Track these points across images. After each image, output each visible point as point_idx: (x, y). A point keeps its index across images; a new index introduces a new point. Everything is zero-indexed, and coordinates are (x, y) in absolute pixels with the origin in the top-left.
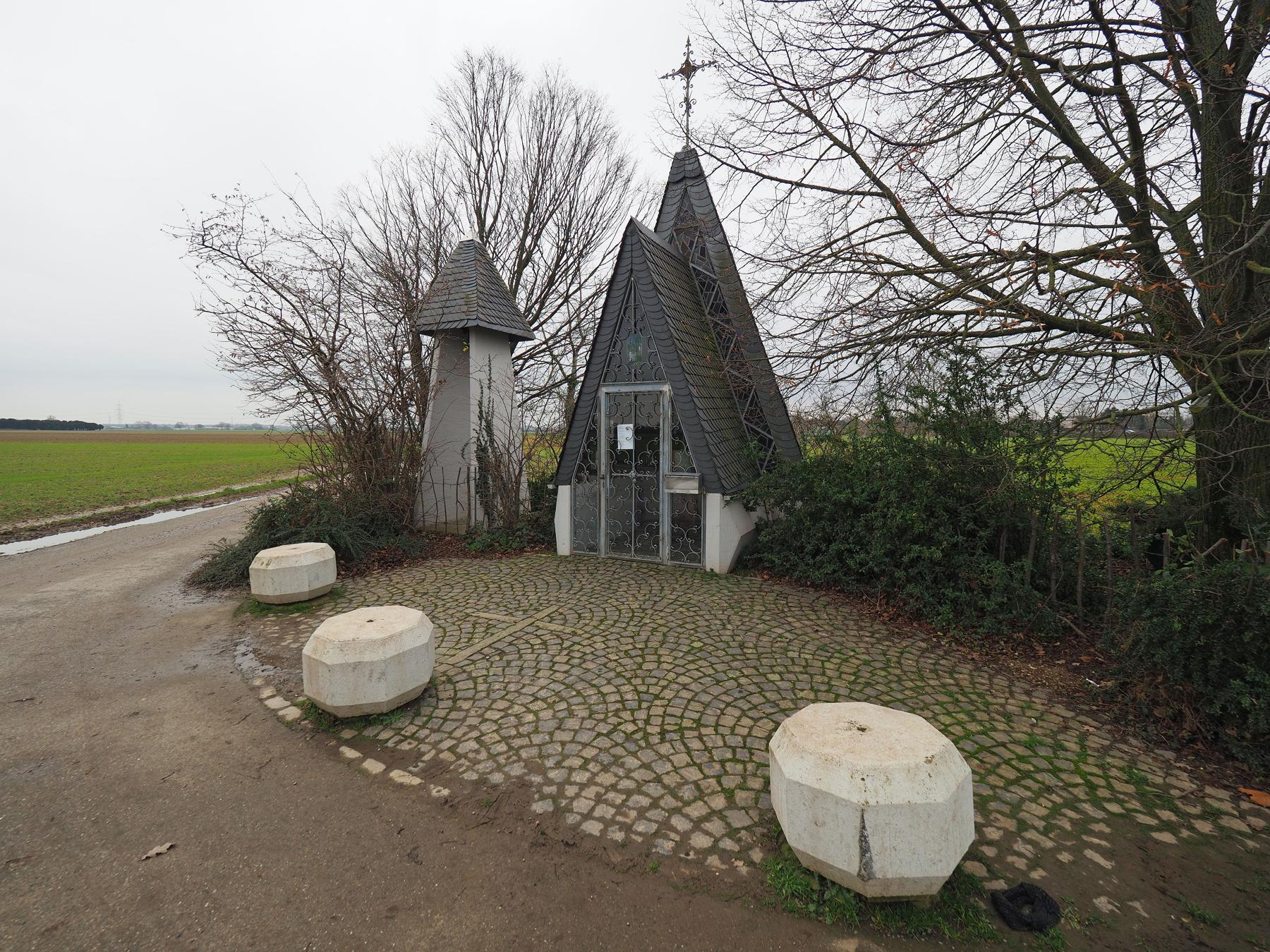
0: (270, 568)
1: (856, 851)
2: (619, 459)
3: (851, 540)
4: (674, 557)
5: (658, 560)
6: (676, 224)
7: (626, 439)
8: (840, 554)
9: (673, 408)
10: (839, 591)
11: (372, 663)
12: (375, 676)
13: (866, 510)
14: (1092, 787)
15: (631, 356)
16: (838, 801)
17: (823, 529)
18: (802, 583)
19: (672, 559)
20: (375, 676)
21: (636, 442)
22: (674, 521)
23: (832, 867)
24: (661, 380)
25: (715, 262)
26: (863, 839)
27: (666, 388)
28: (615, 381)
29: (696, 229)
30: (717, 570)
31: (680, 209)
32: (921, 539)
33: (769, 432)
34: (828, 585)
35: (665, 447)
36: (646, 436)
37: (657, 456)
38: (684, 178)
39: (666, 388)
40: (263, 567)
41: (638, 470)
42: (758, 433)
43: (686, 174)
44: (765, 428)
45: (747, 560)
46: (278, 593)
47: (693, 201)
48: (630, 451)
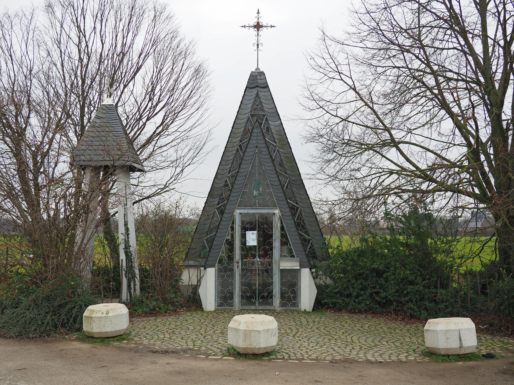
0: (109, 315)
1: (459, 341)
2: (247, 251)
3: (377, 287)
4: (282, 305)
5: (272, 308)
6: (251, 111)
7: (252, 238)
8: (371, 295)
9: (282, 223)
10: (372, 313)
11: (272, 329)
12: (273, 334)
13: (385, 272)
14: (492, 344)
15: (255, 193)
16: (453, 331)
17: (361, 283)
18: (353, 311)
19: (282, 306)
20: (273, 334)
21: (258, 241)
22: (282, 284)
23: (452, 349)
24: (274, 206)
25: (275, 136)
26: (460, 338)
27: (277, 211)
28: (246, 206)
29: (264, 116)
30: (308, 310)
31: (254, 104)
32: (411, 283)
33: (308, 235)
34: (369, 311)
35: (277, 244)
36: (265, 238)
37: (271, 249)
38: (257, 86)
39: (277, 211)
40: (104, 315)
41: (259, 257)
42: (302, 235)
43: (257, 83)
44: (306, 233)
45: (320, 305)
46: (113, 330)
47: (262, 100)
48: (255, 246)
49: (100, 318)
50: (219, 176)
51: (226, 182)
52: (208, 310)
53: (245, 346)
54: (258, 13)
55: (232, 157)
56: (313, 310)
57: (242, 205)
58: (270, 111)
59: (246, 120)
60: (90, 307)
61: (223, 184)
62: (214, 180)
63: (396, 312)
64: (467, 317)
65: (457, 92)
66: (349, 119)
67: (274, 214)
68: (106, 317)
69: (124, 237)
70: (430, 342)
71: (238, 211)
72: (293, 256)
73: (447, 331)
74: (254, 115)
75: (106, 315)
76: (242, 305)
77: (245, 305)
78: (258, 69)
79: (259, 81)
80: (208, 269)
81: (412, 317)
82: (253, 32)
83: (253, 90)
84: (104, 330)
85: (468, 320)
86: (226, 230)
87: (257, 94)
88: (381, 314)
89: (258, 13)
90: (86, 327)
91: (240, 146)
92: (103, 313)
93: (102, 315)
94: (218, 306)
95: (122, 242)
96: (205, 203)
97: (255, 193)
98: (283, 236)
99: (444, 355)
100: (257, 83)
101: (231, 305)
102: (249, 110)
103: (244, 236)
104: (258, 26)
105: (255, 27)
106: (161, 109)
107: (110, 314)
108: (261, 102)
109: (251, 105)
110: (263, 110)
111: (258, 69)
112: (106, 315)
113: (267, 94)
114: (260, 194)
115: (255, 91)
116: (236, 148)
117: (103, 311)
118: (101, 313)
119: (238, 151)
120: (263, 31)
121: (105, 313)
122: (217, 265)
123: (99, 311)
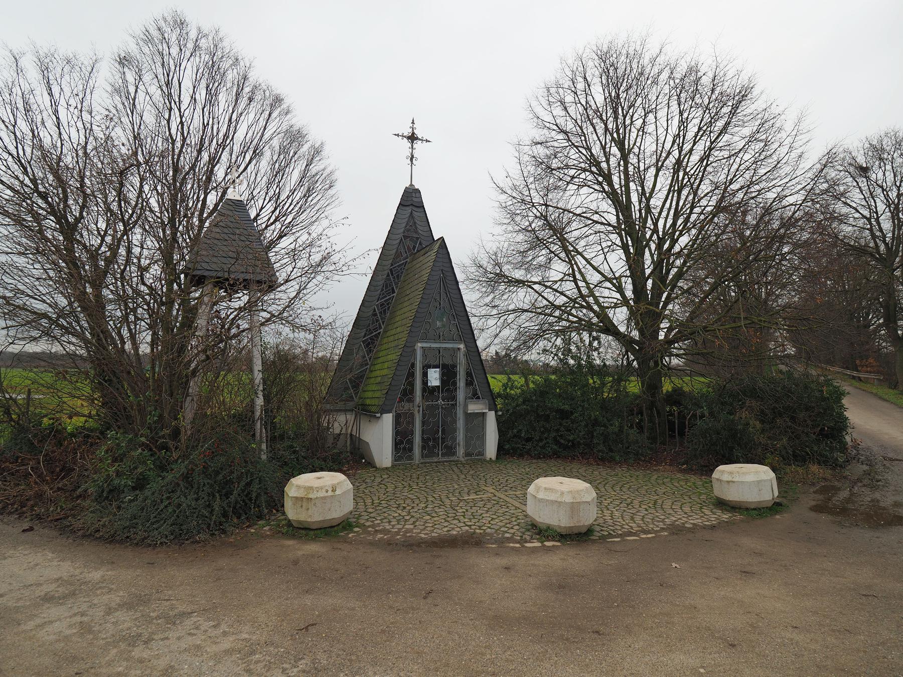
2: (429, 391)
7: (434, 378)
15: (438, 323)
16: (765, 481)
21: (442, 381)
29: (417, 239)
35: (461, 383)
36: (449, 374)
39: (462, 346)
40: (330, 493)
43: (411, 201)
45: (502, 450)
49: (324, 498)
51: (375, 310)
52: (384, 466)
53: (572, 525)
54: (413, 123)
55: (381, 283)
56: (497, 458)
57: (425, 339)
58: (425, 234)
59: (398, 241)
60: (294, 481)
61: (371, 313)
63: (583, 454)
66: (291, 278)
67: (459, 349)
68: (332, 496)
70: (719, 492)
71: (419, 345)
72: (478, 398)
73: (759, 482)
74: (408, 237)
75: (332, 494)
76: (422, 457)
77: (427, 456)
78: (411, 185)
79: (414, 199)
80: (385, 415)
81: (603, 459)
82: (406, 143)
83: (407, 208)
87: (411, 213)
88: (565, 458)
89: (413, 123)
90: (292, 512)
91: (391, 270)
92: (327, 491)
94: (396, 460)
97: (438, 323)
98: (469, 374)
99: (755, 509)
100: (411, 201)
101: (410, 458)
102: (402, 230)
103: (425, 375)
104: (412, 138)
105: (409, 138)
107: (338, 492)
108: (415, 223)
109: (404, 225)
110: (416, 232)
111: (411, 185)
112: (332, 494)
113: (398, 221)
114: (444, 326)
115: (409, 210)
116: (386, 272)
118: (324, 491)
119: (388, 275)
120: (418, 145)
121: (330, 490)
123: (322, 488)
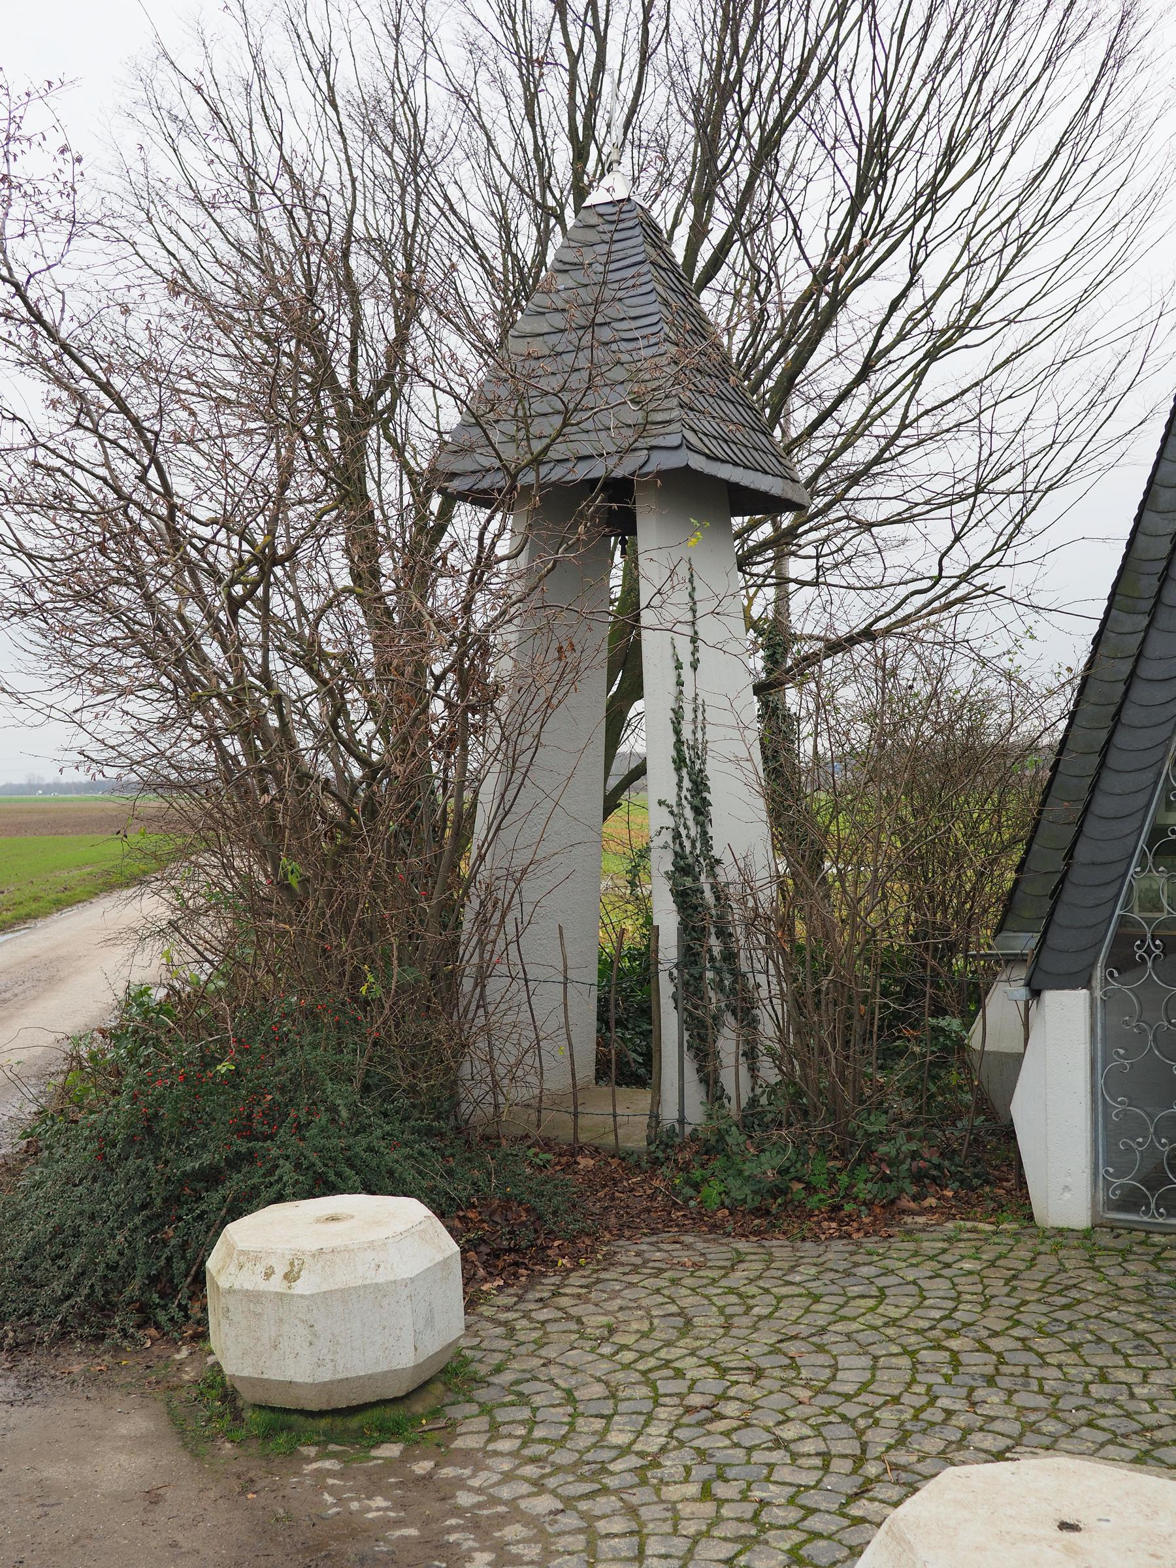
0: (301, 1287)
40: (276, 1284)
46: (325, 1375)
50: (1165, 497)
62: (1138, 520)
64: (399, 1189)
65: (541, 67)
68: (280, 1296)
69: (670, 822)
84: (272, 1375)
85: (410, 1212)
86: (1150, 776)
92: (269, 1273)
93: (263, 1286)
95: (658, 842)
96: (1097, 640)
106: (970, 174)
117: (272, 1261)
118: (260, 1268)
121: (281, 1270)
122: (1098, 973)
